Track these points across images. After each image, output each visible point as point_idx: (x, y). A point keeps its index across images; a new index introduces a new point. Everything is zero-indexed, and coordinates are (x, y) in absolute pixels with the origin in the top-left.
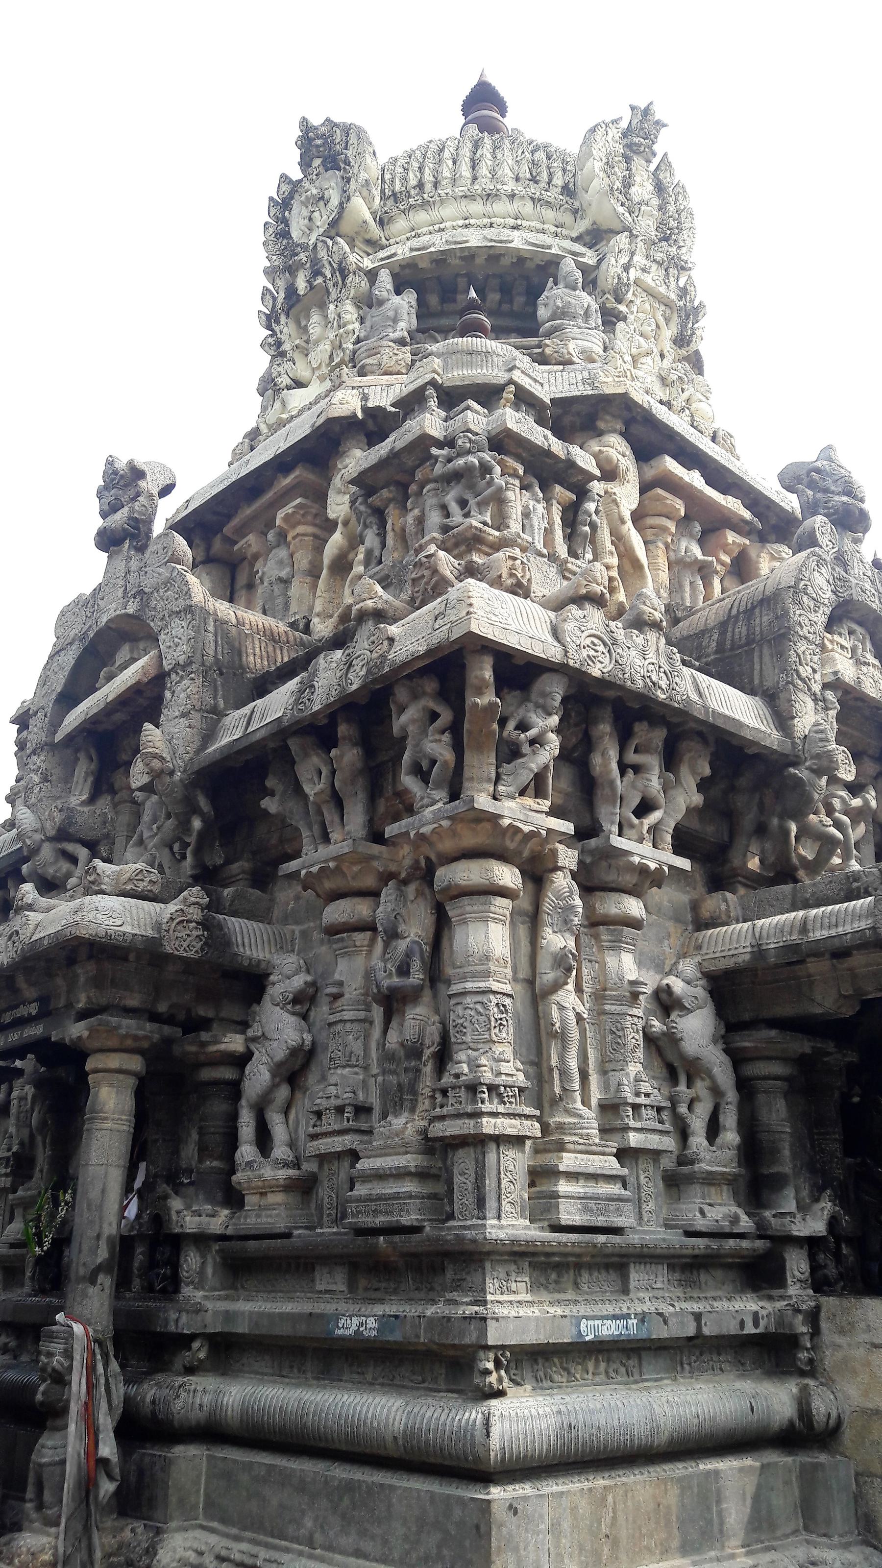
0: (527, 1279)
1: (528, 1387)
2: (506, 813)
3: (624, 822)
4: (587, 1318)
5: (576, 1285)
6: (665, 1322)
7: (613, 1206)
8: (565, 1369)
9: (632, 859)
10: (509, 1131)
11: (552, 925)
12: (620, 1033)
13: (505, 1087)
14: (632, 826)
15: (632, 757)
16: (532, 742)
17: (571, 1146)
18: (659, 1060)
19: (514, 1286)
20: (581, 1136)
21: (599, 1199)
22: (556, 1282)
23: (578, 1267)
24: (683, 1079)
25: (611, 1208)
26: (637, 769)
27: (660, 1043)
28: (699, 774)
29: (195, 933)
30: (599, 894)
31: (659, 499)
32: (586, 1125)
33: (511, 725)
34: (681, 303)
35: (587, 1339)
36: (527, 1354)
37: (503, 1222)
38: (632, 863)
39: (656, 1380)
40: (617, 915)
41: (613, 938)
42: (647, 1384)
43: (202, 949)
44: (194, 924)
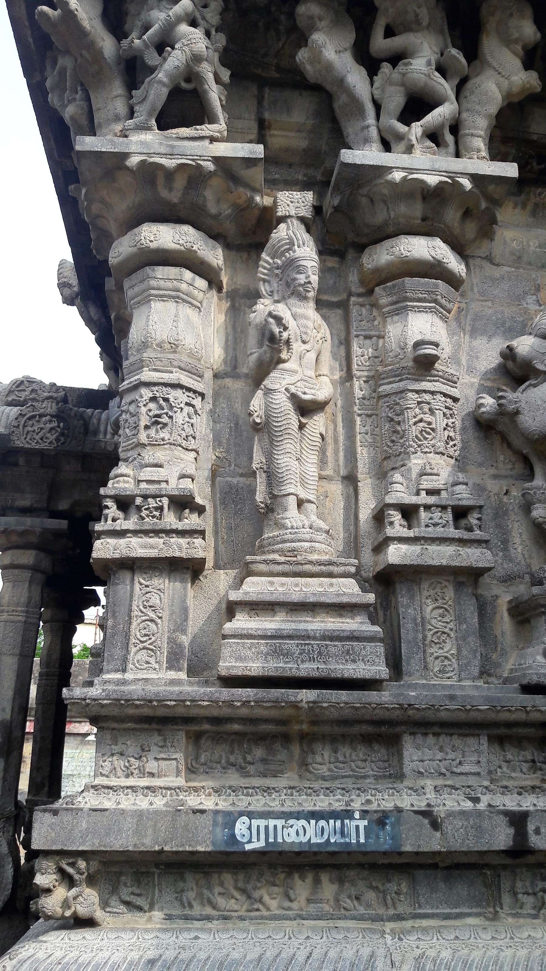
0: (179, 756)
1: (157, 915)
2: (133, 148)
3: (389, 138)
4: (251, 815)
5: (304, 764)
6: (435, 825)
7: (335, 647)
8: (243, 891)
9: (389, 177)
10: (141, 553)
11: (271, 294)
12: (400, 418)
13: (145, 497)
14: (400, 137)
17: (263, 567)
18: (509, 453)
19: (152, 766)
20: (281, 552)
21: (309, 637)
22: (264, 761)
23: (308, 739)
25: (332, 650)
27: (500, 427)
28: (516, 41)
29: (49, 426)
32: (290, 537)
35: (248, 847)
36: (157, 865)
37: (129, 676)
38: (392, 184)
39: (447, 917)
40: (390, 264)
41: (395, 298)
42: (425, 923)
43: (57, 440)
44: (48, 418)
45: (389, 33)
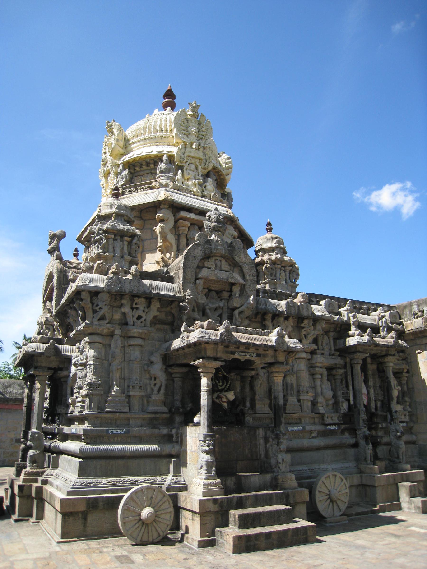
15: (134, 306)
16: (100, 308)
24: (153, 379)
26: (137, 309)
30: (130, 338)
31: (181, 223)
33: (95, 305)
34: (204, 158)
45: (136, 304)
